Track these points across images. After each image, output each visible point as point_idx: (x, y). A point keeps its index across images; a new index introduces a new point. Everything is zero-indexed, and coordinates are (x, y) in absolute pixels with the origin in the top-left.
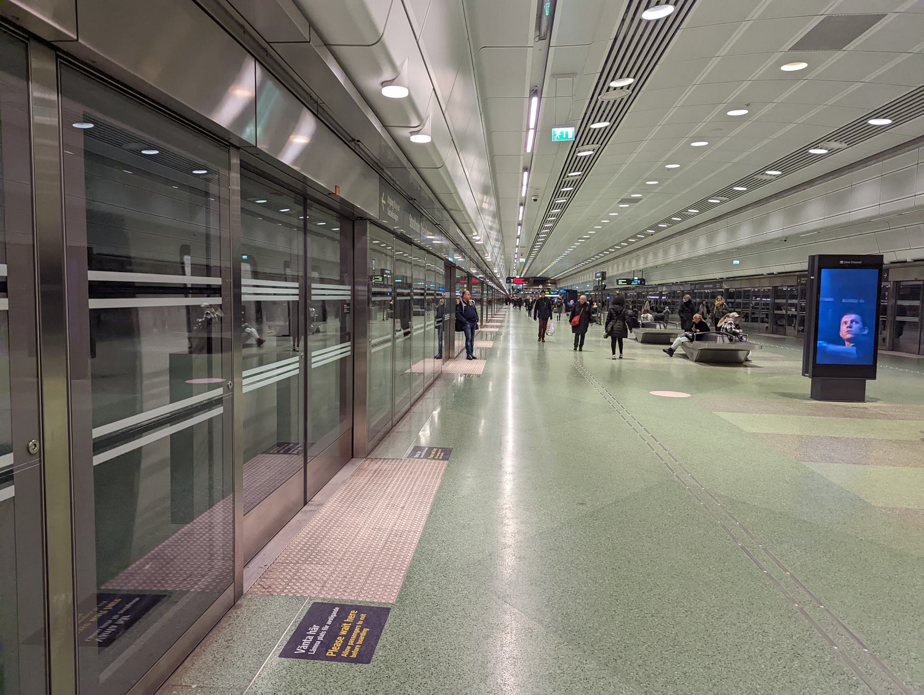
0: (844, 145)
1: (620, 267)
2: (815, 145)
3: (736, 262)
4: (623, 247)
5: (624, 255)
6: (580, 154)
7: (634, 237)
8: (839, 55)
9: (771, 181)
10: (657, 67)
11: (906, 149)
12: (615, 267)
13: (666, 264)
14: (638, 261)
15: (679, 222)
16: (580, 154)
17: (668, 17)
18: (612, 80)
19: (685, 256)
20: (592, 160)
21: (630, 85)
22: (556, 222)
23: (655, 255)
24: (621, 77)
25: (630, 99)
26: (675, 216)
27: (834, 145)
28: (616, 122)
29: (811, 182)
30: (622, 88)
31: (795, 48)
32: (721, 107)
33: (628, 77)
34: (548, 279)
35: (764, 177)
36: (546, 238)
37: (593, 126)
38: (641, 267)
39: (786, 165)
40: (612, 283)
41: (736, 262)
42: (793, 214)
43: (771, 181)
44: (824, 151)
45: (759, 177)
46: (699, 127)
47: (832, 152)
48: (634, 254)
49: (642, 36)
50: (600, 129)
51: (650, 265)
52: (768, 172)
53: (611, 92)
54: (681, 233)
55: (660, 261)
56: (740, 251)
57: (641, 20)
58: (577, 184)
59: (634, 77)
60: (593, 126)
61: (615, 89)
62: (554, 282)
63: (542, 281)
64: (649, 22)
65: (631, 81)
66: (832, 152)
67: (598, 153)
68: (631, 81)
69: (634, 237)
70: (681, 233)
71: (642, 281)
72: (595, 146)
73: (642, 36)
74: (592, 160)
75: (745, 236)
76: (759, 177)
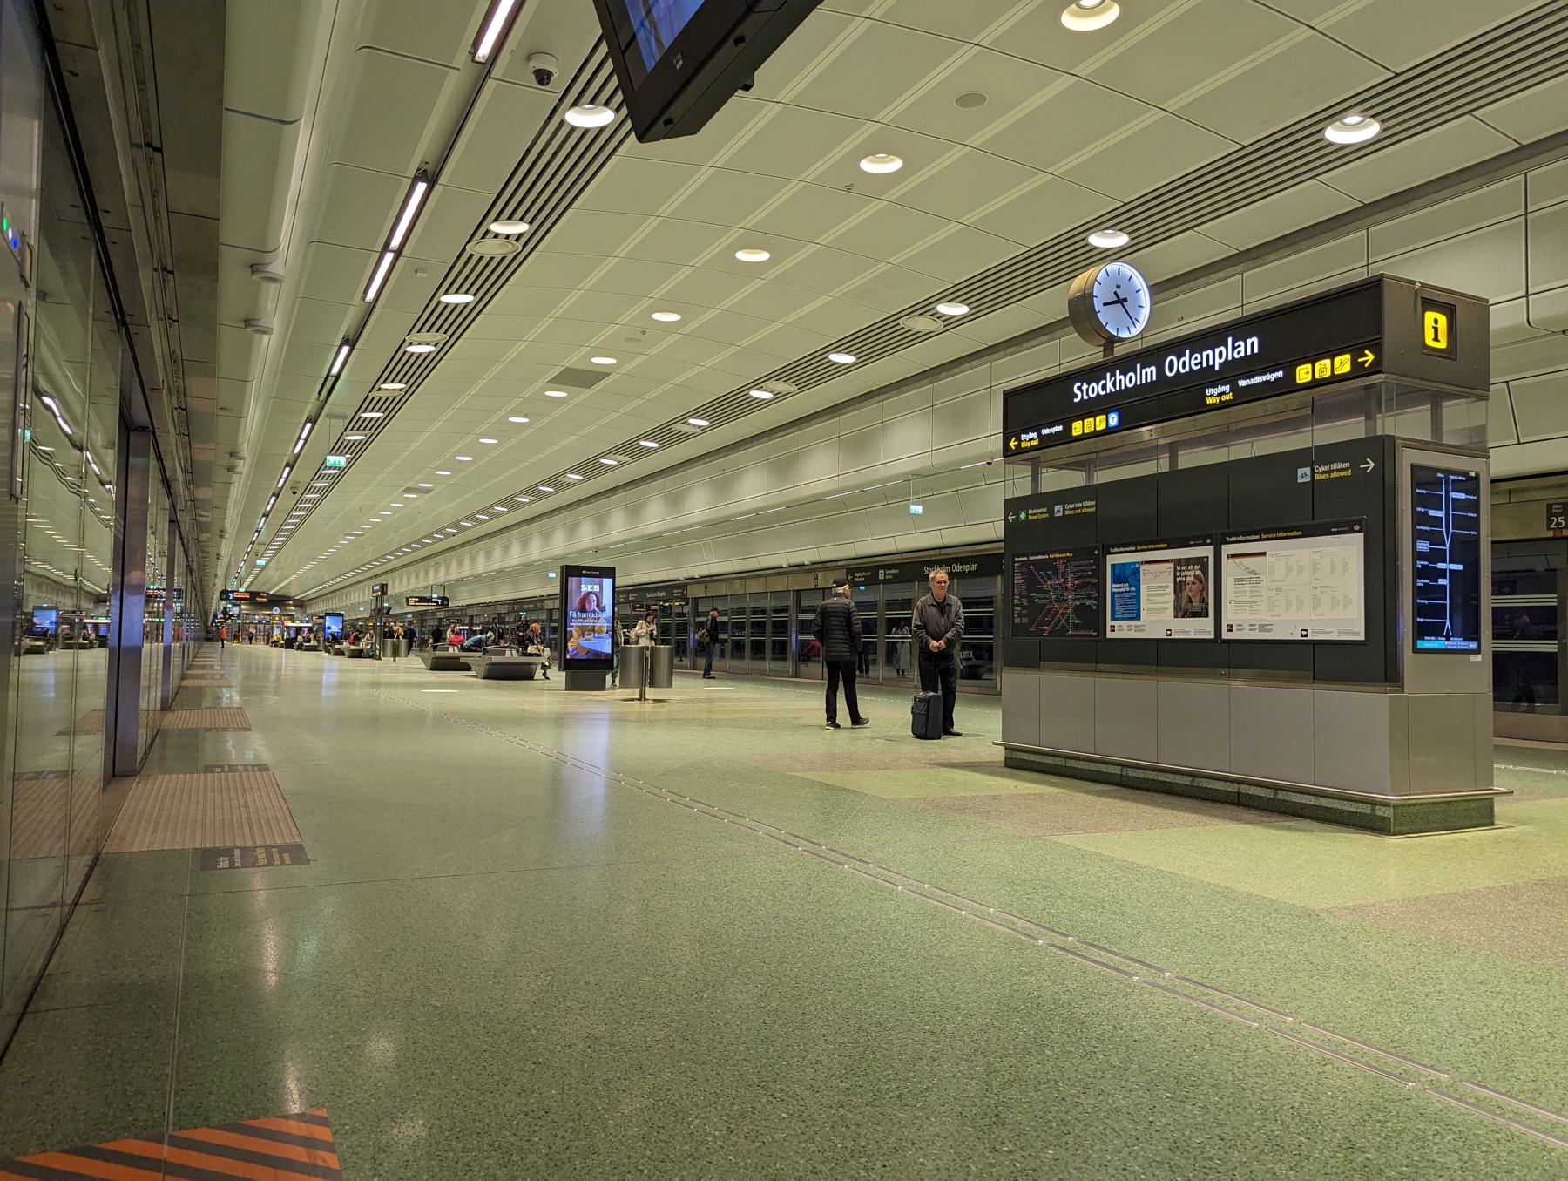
0: (793, 388)
1: (413, 580)
2: (758, 384)
3: (916, 509)
4: (415, 550)
5: (463, 545)
6: (411, 349)
7: (429, 536)
8: (588, 392)
9: (693, 435)
10: (569, 211)
11: (1214, 277)
12: (422, 575)
13: (525, 565)
14: (436, 571)
15: (550, 494)
16: (411, 349)
17: (602, 130)
18: (496, 220)
19: (497, 566)
20: (429, 362)
21: (521, 235)
22: (310, 511)
23: (460, 563)
24: (510, 218)
25: (517, 261)
26: (543, 483)
27: (783, 387)
28: (485, 296)
29: (613, 490)
30: (508, 237)
31: (550, 382)
32: (584, 350)
33: (521, 219)
34: (289, 599)
35: (685, 428)
36: (293, 532)
37: (447, 299)
38: (441, 580)
39: (874, 341)
40: (399, 604)
41: (916, 509)
42: (723, 487)
43: (693, 435)
44: (768, 396)
45: (678, 427)
46: (484, 427)
47: (779, 397)
48: (432, 561)
49: (555, 154)
50: (456, 306)
51: (454, 576)
52: (691, 421)
53: (489, 241)
54: (491, 535)
55: (467, 572)
56: (652, 542)
57: (562, 123)
58: (391, 407)
59: (531, 223)
60: (447, 299)
61: (496, 236)
62: (301, 604)
63: (279, 601)
64: (573, 129)
65: (523, 227)
66: (779, 397)
67: (443, 350)
68: (523, 227)
69: (429, 536)
70: (491, 535)
71: (445, 600)
72: (441, 337)
73: (555, 154)
74: (429, 362)
75: (699, 506)
76: (678, 427)
